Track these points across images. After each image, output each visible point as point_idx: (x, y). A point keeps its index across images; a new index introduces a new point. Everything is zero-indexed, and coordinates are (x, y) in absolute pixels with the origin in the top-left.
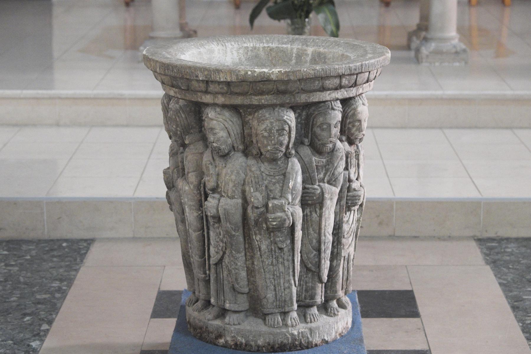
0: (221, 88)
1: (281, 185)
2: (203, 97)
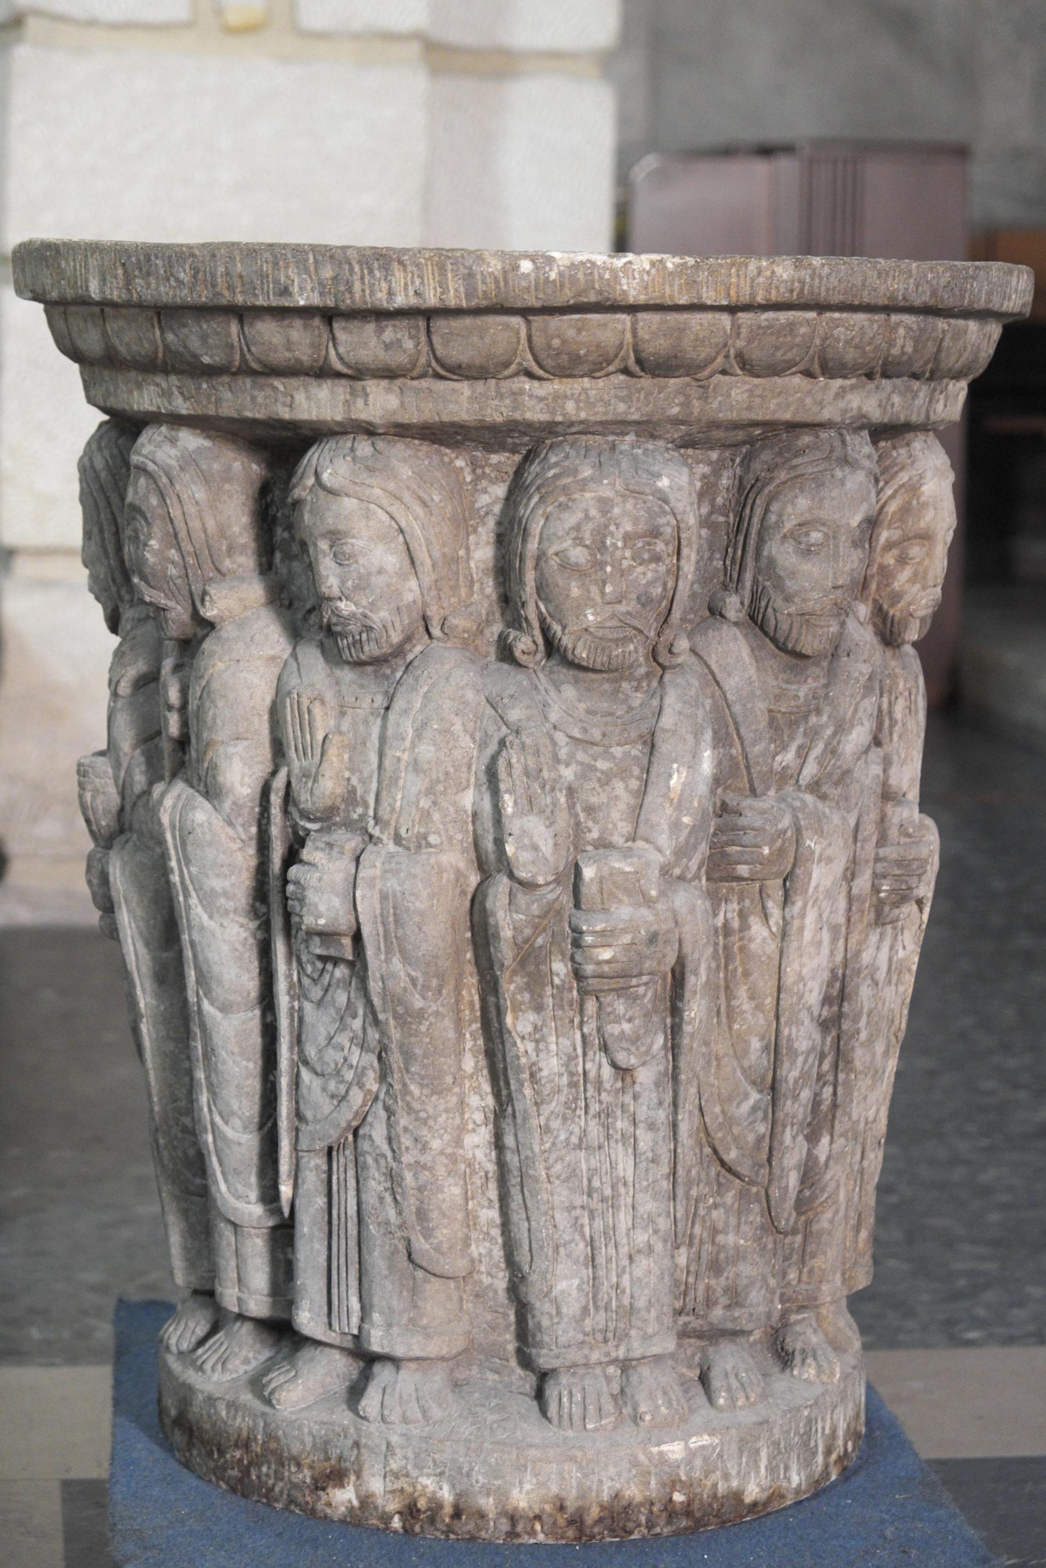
0: (387, 347)
1: (634, 784)
2: (300, 397)
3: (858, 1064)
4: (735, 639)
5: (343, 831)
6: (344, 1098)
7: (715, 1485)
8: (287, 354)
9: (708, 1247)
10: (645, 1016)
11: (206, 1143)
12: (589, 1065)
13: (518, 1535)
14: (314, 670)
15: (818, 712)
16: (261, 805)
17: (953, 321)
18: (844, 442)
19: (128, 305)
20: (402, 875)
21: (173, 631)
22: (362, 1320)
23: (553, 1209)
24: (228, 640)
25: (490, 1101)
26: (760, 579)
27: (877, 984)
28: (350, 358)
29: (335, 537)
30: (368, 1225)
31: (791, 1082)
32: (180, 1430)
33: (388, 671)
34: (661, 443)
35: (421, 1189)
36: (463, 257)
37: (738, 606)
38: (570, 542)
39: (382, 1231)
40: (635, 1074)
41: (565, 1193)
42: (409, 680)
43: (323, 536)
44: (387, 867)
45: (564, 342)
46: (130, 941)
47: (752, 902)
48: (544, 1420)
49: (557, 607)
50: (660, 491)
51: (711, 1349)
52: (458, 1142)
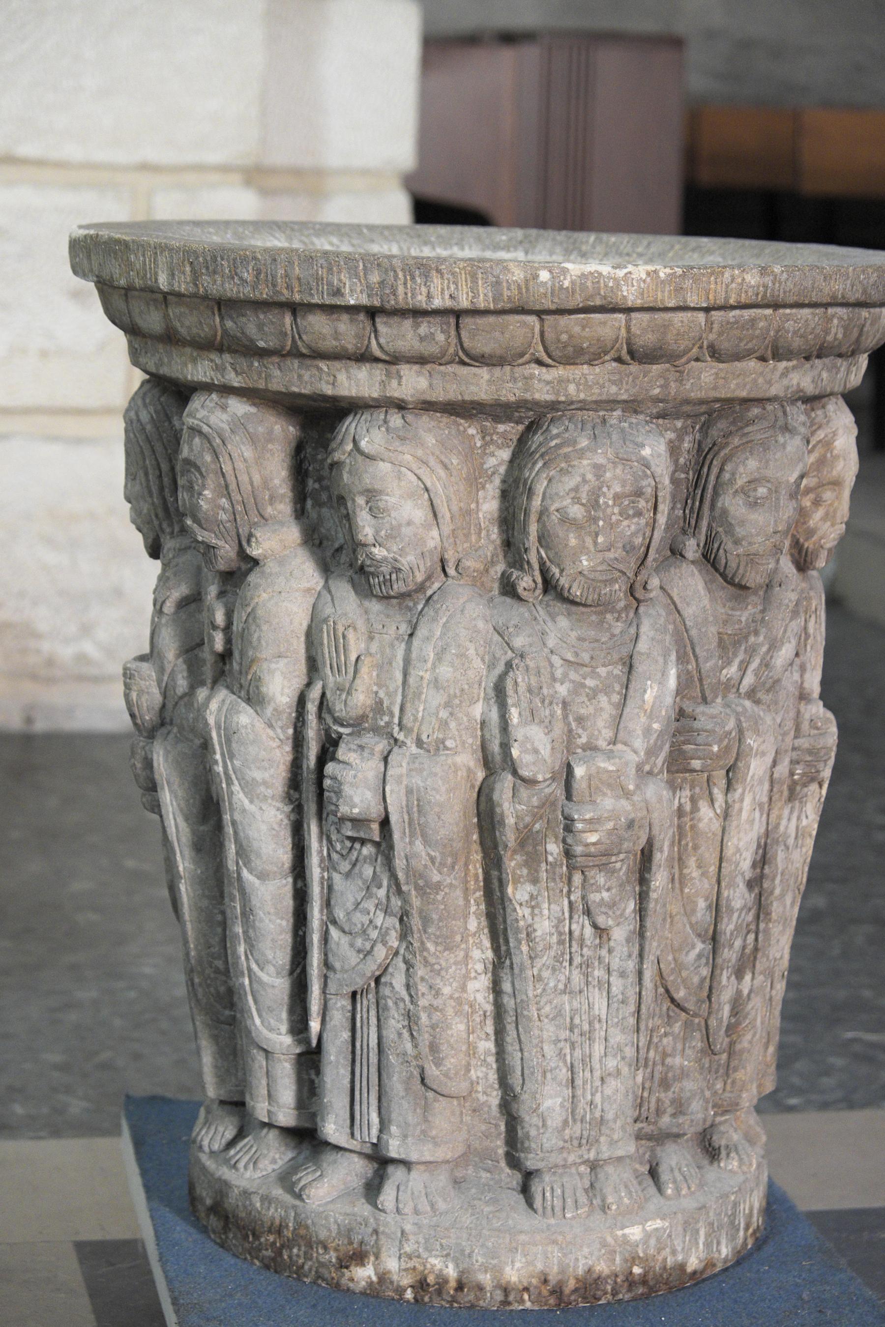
0: (422, 339)
1: (616, 698)
2: (342, 377)
3: (774, 916)
4: (693, 575)
5: (371, 734)
6: (369, 953)
7: (665, 1260)
8: (334, 343)
9: (659, 1068)
10: (620, 886)
11: (242, 985)
12: (574, 927)
13: (509, 1303)
14: (347, 603)
15: (756, 633)
16: (297, 711)
17: (872, 310)
18: (785, 413)
19: (195, 295)
20: (425, 773)
21: (222, 566)
22: (381, 1131)
23: (542, 1042)
24: (271, 574)
25: (490, 954)
26: (714, 525)
27: (787, 848)
28: (390, 348)
29: (371, 494)
30: (388, 1055)
31: (728, 934)
32: (219, 1219)
33: (411, 604)
34: (641, 417)
35: (433, 1027)
36: (492, 268)
37: (695, 547)
38: (569, 501)
39: (401, 1060)
40: (611, 933)
41: (552, 1029)
42: (430, 612)
43: (361, 493)
44: (412, 766)
45: (571, 337)
46: (171, 816)
47: (701, 789)
48: (530, 1211)
49: (556, 553)
50: (644, 458)
51: (658, 1148)
52: (463, 988)
